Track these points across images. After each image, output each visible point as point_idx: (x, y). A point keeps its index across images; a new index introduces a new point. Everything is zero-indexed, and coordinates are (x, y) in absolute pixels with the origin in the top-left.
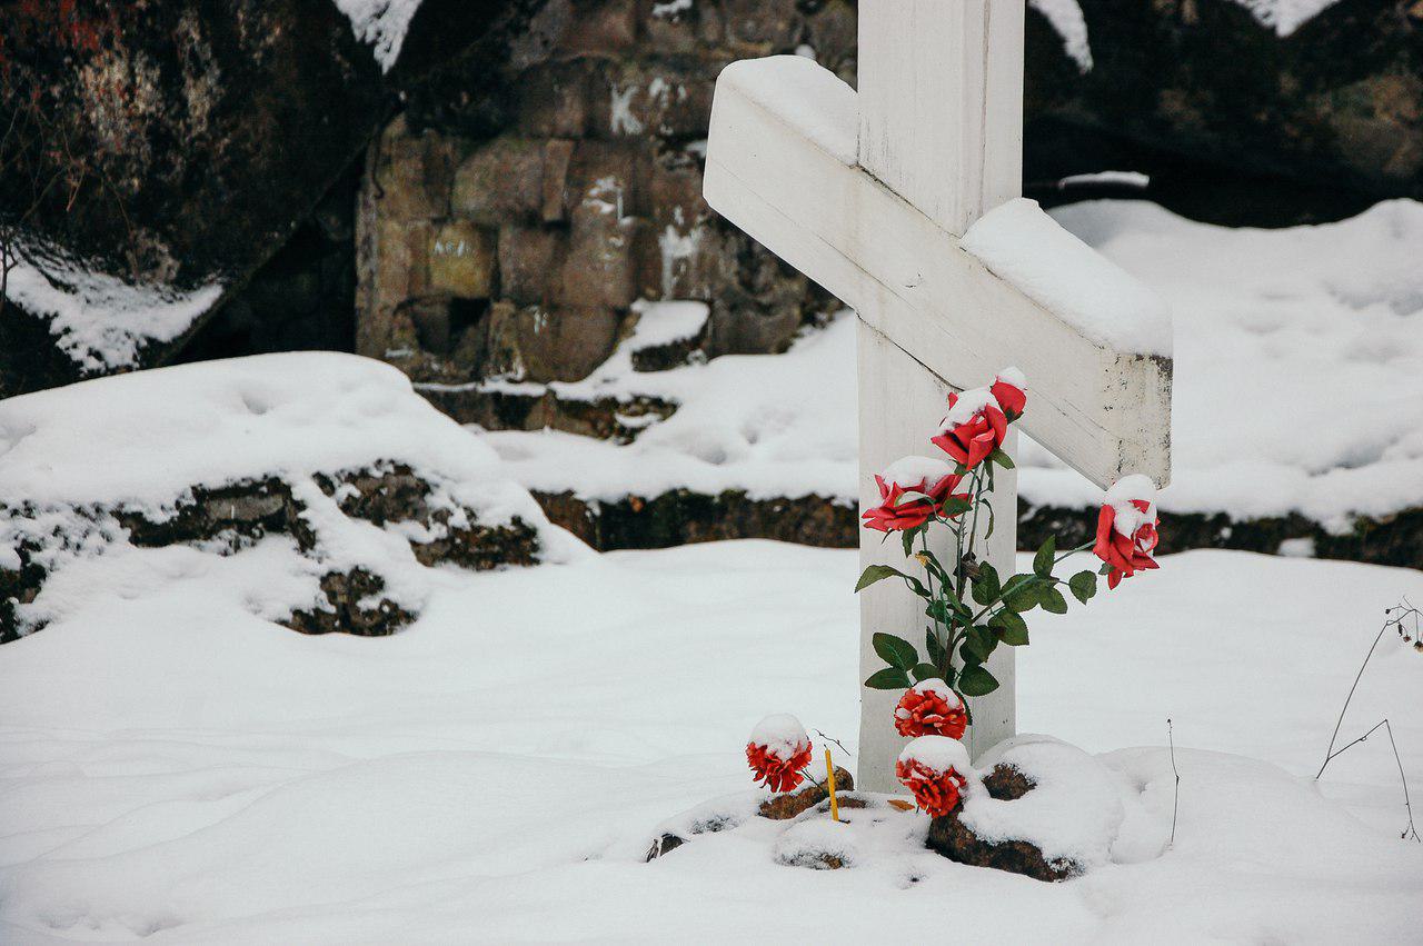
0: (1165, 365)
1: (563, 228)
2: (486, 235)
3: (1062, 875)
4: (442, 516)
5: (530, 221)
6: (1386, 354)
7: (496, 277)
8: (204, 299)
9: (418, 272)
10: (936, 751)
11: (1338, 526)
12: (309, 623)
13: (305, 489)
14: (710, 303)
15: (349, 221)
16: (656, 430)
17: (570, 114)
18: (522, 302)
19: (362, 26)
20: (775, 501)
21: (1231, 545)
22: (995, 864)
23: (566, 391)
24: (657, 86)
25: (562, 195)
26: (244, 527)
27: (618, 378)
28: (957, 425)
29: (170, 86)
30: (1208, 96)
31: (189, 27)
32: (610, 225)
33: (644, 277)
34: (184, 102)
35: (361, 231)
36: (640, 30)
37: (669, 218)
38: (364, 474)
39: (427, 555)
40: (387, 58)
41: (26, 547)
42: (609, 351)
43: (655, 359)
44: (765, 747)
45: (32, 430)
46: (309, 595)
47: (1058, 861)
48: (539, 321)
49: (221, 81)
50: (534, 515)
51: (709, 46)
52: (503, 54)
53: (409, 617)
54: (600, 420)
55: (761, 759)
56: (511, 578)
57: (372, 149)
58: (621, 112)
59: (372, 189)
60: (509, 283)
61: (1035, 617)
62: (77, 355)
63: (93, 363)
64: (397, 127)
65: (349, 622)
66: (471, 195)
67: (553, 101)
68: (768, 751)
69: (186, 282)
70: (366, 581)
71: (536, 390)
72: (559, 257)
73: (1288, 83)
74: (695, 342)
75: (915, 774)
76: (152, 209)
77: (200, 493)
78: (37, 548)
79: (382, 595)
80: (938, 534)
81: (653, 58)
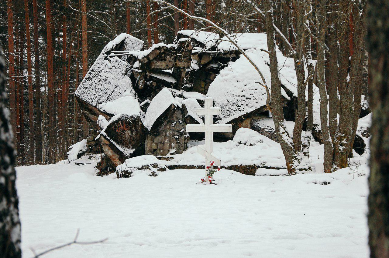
1: (163, 143)
2: (157, 144)
4: (159, 167)
5: (161, 143)
6: (230, 153)
8: (134, 150)
9: (151, 147)
10: (210, 179)
11: (227, 167)
12: (151, 176)
13: (150, 166)
16: (172, 160)
17: (164, 134)
18: (160, 149)
19: (146, 127)
23: (164, 157)
25: (163, 141)
26: (145, 169)
27: (169, 156)
29: (132, 133)
32: (168, 143)
33: (170, 147)
36: (170, 127)
39: (158, 170)
43: (172, 154)
46: (151, 174)
50: (166, 167)
53: (157, 175)
54: (167, 159)
55: (202, 180)
56: (164, 172)
58: (168, 134)
60: (159, 148)
61: (214, 173)
63: (126, 155)
64: (149, 135)
65: (153, 175)
66: (156, 141)
67: (162, 133)
69: (133, 148)
70: (154, 172)
71: (162, 157)
72: (163, 146)
74: (175, 153)
77: (142, 166)
80: (210, 168)
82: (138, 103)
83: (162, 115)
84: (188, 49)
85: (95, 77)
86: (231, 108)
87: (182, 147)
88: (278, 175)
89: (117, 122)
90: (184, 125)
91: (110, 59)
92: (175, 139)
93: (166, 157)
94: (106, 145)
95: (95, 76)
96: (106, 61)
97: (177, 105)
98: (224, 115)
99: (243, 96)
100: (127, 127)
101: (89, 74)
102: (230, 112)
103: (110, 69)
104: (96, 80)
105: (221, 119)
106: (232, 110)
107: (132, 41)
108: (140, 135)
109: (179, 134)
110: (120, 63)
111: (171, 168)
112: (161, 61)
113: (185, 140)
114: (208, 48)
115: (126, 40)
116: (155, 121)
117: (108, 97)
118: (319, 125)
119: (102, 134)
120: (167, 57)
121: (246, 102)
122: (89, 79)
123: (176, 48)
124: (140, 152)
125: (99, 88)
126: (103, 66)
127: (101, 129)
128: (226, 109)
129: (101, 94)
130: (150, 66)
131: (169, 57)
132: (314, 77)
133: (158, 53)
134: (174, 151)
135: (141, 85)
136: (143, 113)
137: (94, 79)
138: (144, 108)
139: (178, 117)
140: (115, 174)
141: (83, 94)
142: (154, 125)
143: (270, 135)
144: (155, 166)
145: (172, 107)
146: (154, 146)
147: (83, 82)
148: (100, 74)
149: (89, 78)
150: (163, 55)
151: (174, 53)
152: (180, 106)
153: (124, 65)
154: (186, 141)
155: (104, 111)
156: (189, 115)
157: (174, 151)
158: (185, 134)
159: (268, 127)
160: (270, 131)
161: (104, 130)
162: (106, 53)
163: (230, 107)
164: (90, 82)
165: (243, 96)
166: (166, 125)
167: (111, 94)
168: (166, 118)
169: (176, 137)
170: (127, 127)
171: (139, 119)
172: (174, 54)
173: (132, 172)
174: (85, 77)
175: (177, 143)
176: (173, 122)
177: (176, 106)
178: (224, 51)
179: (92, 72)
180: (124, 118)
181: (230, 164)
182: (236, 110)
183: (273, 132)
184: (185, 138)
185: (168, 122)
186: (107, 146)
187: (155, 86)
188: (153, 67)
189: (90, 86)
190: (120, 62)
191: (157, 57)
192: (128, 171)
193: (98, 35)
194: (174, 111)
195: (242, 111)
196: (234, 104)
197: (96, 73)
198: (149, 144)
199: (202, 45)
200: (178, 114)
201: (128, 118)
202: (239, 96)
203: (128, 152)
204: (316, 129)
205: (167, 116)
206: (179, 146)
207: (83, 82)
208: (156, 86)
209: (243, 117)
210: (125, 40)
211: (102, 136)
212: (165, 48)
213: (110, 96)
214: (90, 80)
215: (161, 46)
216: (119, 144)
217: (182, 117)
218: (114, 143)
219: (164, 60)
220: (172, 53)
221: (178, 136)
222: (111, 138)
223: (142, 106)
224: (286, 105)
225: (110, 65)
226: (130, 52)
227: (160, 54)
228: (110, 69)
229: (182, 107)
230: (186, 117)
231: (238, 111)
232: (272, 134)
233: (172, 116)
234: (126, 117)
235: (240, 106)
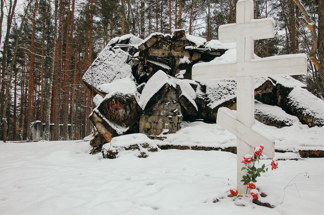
0: (274, 143)
1: (157, 123)
2: (150, 123)
3: (273, 207)
4: (150, 147)
5: (154, 122)
7: (151, 127)
8: (128, 128)
11: (223, 148)
12: (140, 157)
13: (139, 145)
14: (169, 129)
15: (139, 122)
16: (165, 140)
17: (158, 114)
18: (153, 129)
19: (141, 107)
20: (176, 146)
21: (214, 150)
22: (263, 206)
23: (157, 136)
24: (165, 112)
26: (134, 148)
27: (162, 135)
28: (257, 151)
29: (126, 111)
30: (205, 113)
31: (128, 107)
33: (164, 127)
34: (127, 113)
35: (140, 123)
36: (164, 107)
37: (166, 122)
38: (144, 144)
39: (149, 151)
40: (143, 109)
41: (117, 150)
42: (161, 133)
43: (165, 134)
44: (232, 190)
45: (117, 140)
47: (272, 206)
48: (155, 130)
49: (130, 111)
50: (157, 147)
51: (169, 108)
52: (153, 109)
53: (148, 156)
54: (160, 139)
56: (155, 152)
57: (141, 116)
58: (162, 114)
59: (141, 119)
61: (261, 173)
62: (118, 133)
63: (119, 134)
64: (143, 115)
65: (143, 157)
66: (150, 120)
68: (233, 191)
69: (126, 127)
70: (144, 153)
71: (155, 136)
73: (212, 112)
74: (168, 132)
75: (253, 194)
76: (124, 121)
77: (131, 146)
78: (117, 150)
79: (145, 154)
81: (164, 109)
82: (135, 86)
83: (156, 94)
84: (183, 39)
85: (100, 64)
86: (222, 92)
87: (175, 126)
88: (284, 160)
89: (111, 99)
90: (178, 105)
91: (114, 50)
92: (168, 119)
93: (159, 136)
94: (99, 122)
96: (111, 52)
97: (172, 85)
98: (216, 98)
99: (233, 81)
100: (121, 106)
101: (95, 62)
102: (221, 95)
103: (114, 58)
104: (101, 67)
105: (213, 102)
106: (223, 93)
107: (135, 40)
108: (135, 114)
109: (172, 114)
110: (123, 53)
111: (163, 147)
112: (158, 49)
113: (178, 121)
114: (198, 46)
115: (131, 39)
116: (148, 100)
117: (110, 81)
118: (306, 109)
119: (95, 111)
120: (163, 45)
121: (236, 86)
122: (95, 66)
123: (172, 37)
124: (134, 129)
125: (103, 74)
126: (108, 56)
127: (95, 106)
128: (217, 93)
129: (104, 79)
130: (148, 54)
131: (165, 46)
133: (155, 41)
134: (167, 130)
135: (140, 72)
136: (138, 94)
137: (100, 66)
138: (140, 91)
139: (172, 97)
140: (100, 154)
141: (89, 78)
142: (147, 104)
143: (258, 118)
144: (146, 146)
145: (166, 86)
146: (148, 125)
147: (90, 69)
148: (105, 62)
149: (95, 65)
150: (160, 44)
151: (170, 42)
152: (175, 86)
153: (126, 55)
154: (180, 121)
155: (102, 91)
156: (183, 96)
157: (167, 130)
158: (179, 114)
159: (256, 110)
160: (259, 114)
161: (97, 107)
162: (111, 45)
163: (221, 90)
164: (96, 68)
165: (233, 81)
166: (160, 104)
167: (113, 79)
168: (160, 98)
169: (169, 117)
170: (121, 106)
171: (133, 98)
172: (169, 43)
173: (117, 153)
174: (92, 65)
175: (170, 123)
176: (167, 102)
177: (171, 86)
178: (211, 49)
179: (97, 60)
180: (118, 96)
181: (227, 146)
182: (227, 94)
183: (262, 115)
184: (179, 118)
185: (162, 102)
186: (100, 124)
187: (151, 71)
188: (151, 54)
190: (123, 52)
191: (154, 45)
192: (113, 152)
194: (169, 90)
195: (233, 95)
196: (225, 88)
197: (101, 61)
198: (143, 124)
199: (193, 44)
200: (172, 94)
201: (123, 97)
202: (229, 81)
203: (120, 130)
204: (303, 113)
205: (161, 95)
206: (172, 125)
207: (90, 69)
208: (152, 71)
209: (233, 101)
210: (130, 39)
211: (94, 114)
212: (161, 37)
213: (112, 81)
214: (96, 67)
215: (158, 34)
216: (112, 122)
217: (176, 97)
218: (106, 120)
219: (160, 48)
220: (168, 41)
221: (172, 116)
222: (105, 115)
223: (139, 88)
224: (271, 91)
225: (114, 55)
226: (132, 45)
227: (157, 42)
228: (114, 58)
229: (176, 87)
230: (180, 97)
231: (229, 95)
232: (260, 117)
233: (166, 96)
234: (120, 96)
235: (231, 90)
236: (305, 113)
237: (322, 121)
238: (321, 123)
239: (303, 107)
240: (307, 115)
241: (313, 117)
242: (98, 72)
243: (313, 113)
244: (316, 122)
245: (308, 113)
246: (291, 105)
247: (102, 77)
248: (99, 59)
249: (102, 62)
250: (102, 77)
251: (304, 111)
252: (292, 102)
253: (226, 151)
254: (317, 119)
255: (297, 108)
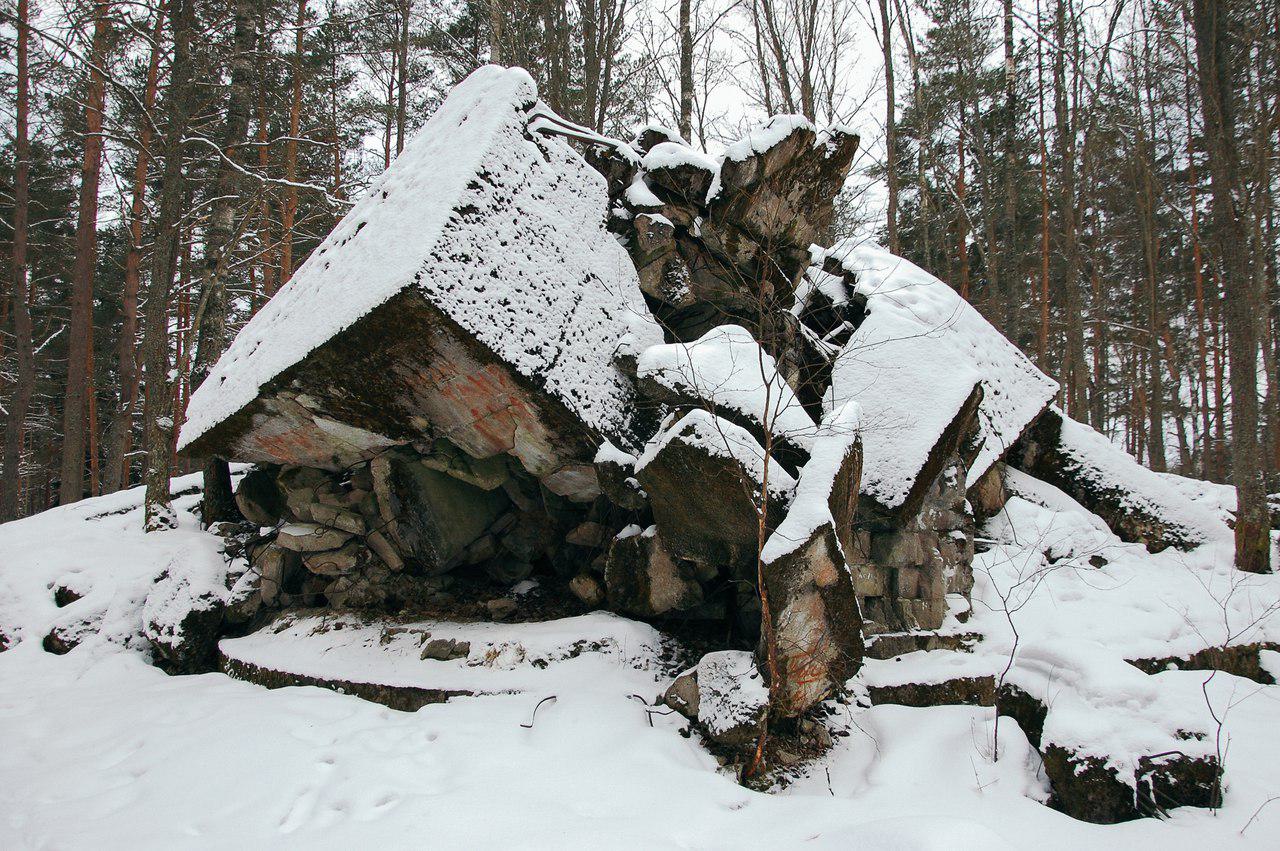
11: (1187, 658)
24: (932, 512)
95: (496, 203)
122: (474, 216)
129: (532, 301)
132: (72, 412)
137: (495, 218)
141: (452, 287)
155: (677, 385)
179: (481, 182)
189: (482, 255)
193: (202, 115)
204: (1121, 505)
214: (478, 219)
236: (1128, 505)
237: (1184, 531)
238: (1183, 537)
239: (1117, 486)
240: (1137, 511)
241: (1156, 518)
242: (495, 256)
243: (1154, 507)
244: (1166, 535)
245: (1138, 507)
246: (1077, 478)
247: (519, 291)
248: (487, 174)
249: (502, 199)
250: (519, 291)
251: (1122, 499)
252: (1078, 466)
253: (296, 685)
254: (1167, 526)
255: (1098, 486)
